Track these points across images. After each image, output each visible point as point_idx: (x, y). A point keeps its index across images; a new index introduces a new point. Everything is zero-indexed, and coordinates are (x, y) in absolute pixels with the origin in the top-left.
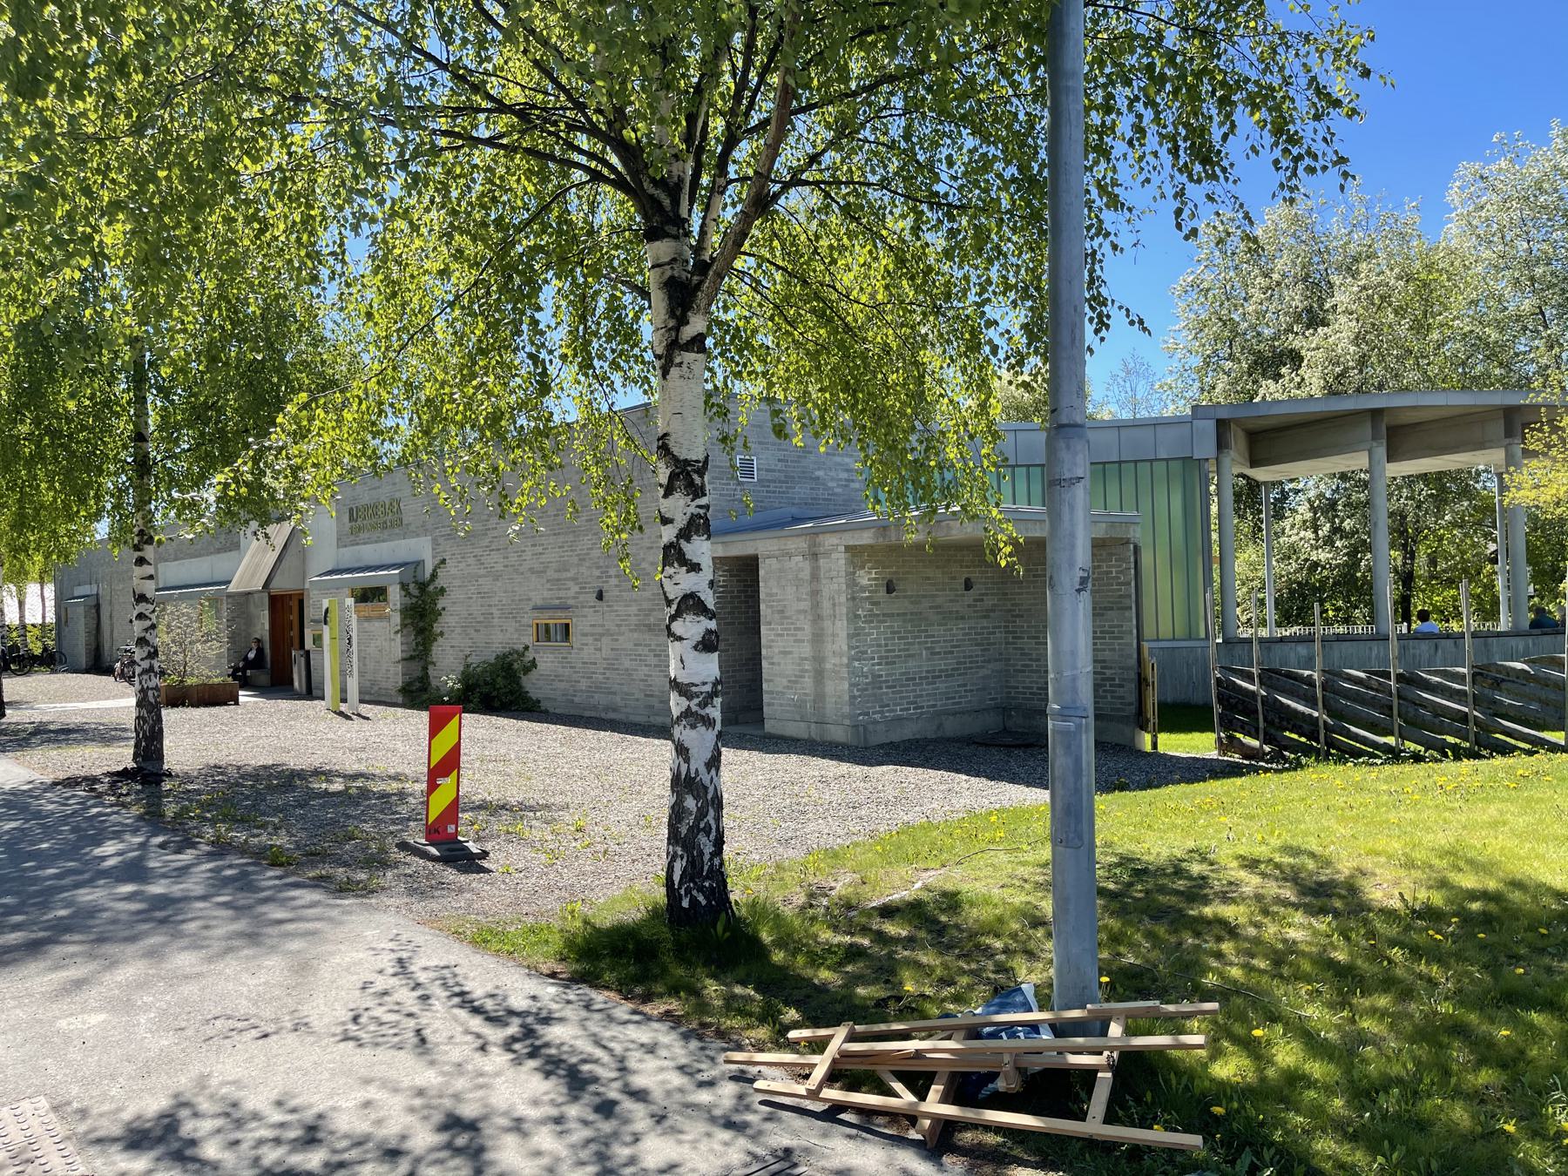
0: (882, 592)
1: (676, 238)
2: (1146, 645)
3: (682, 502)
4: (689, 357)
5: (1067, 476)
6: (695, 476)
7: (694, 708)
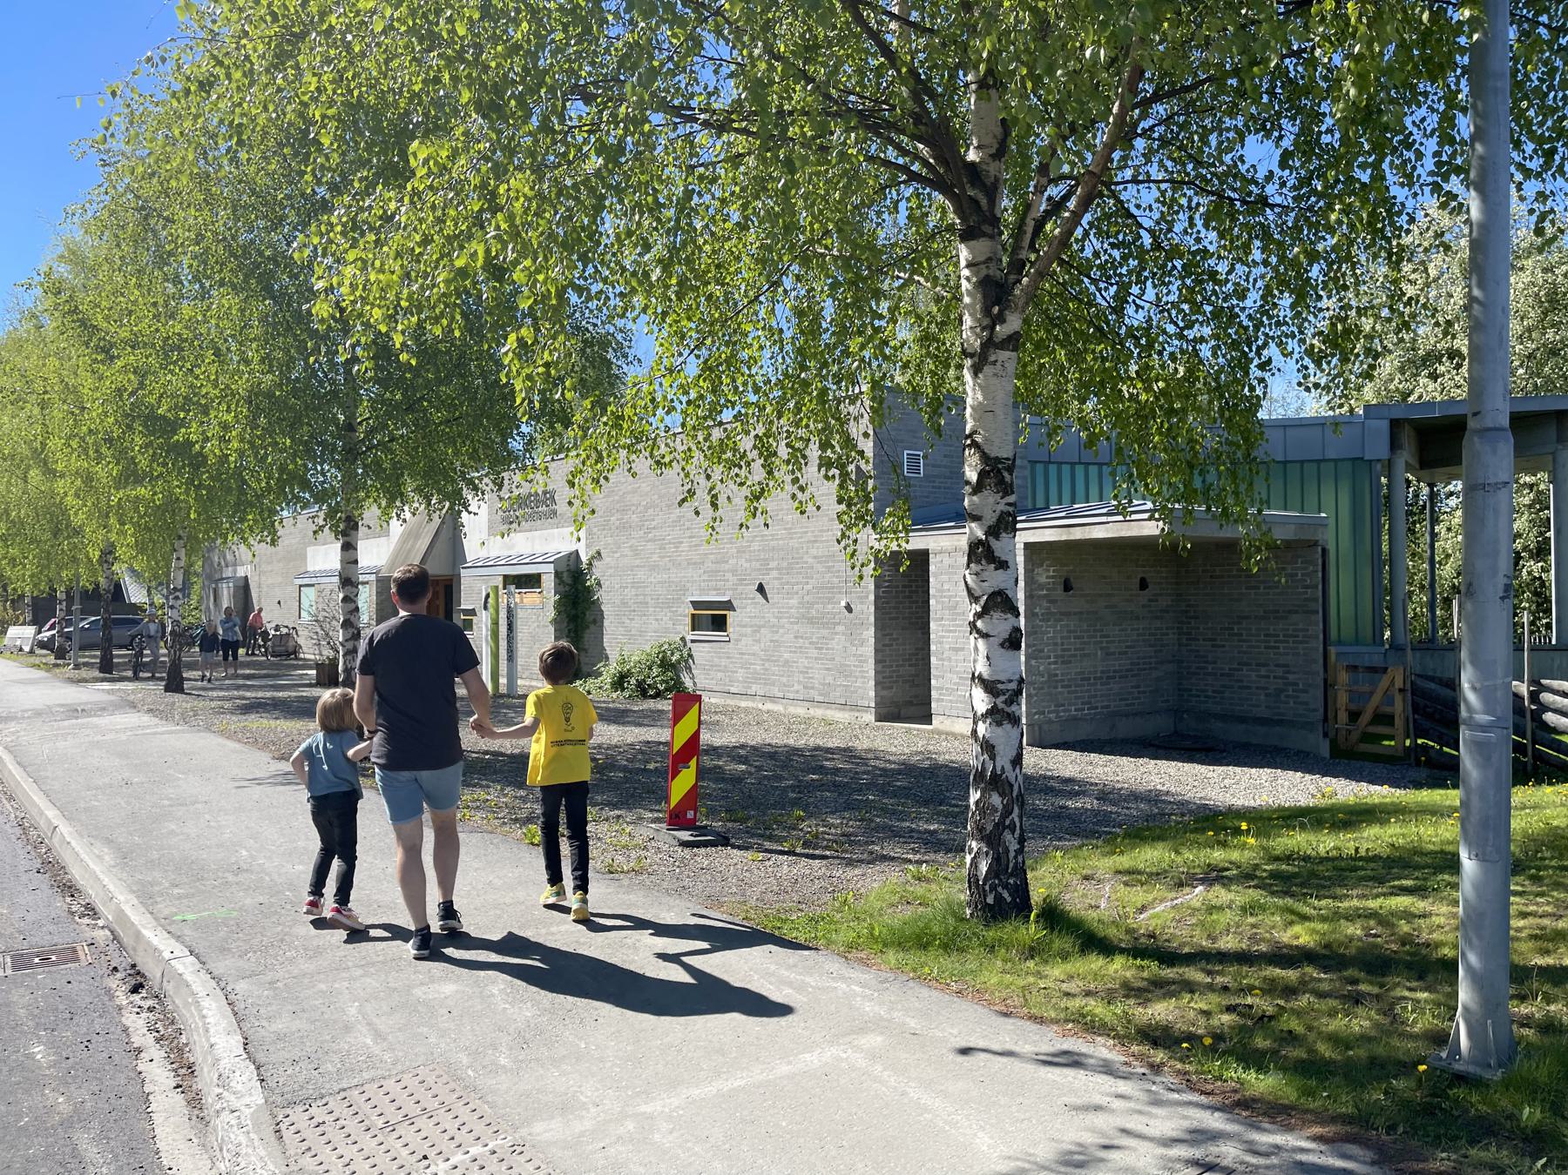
0: (1060, 591)
1: (992, 237)
2: (1332, 650)
3: (991, 500)
4: (1003, 355)
5: (1492, 481)
6: (1006, 474)
7: (1001, 706)
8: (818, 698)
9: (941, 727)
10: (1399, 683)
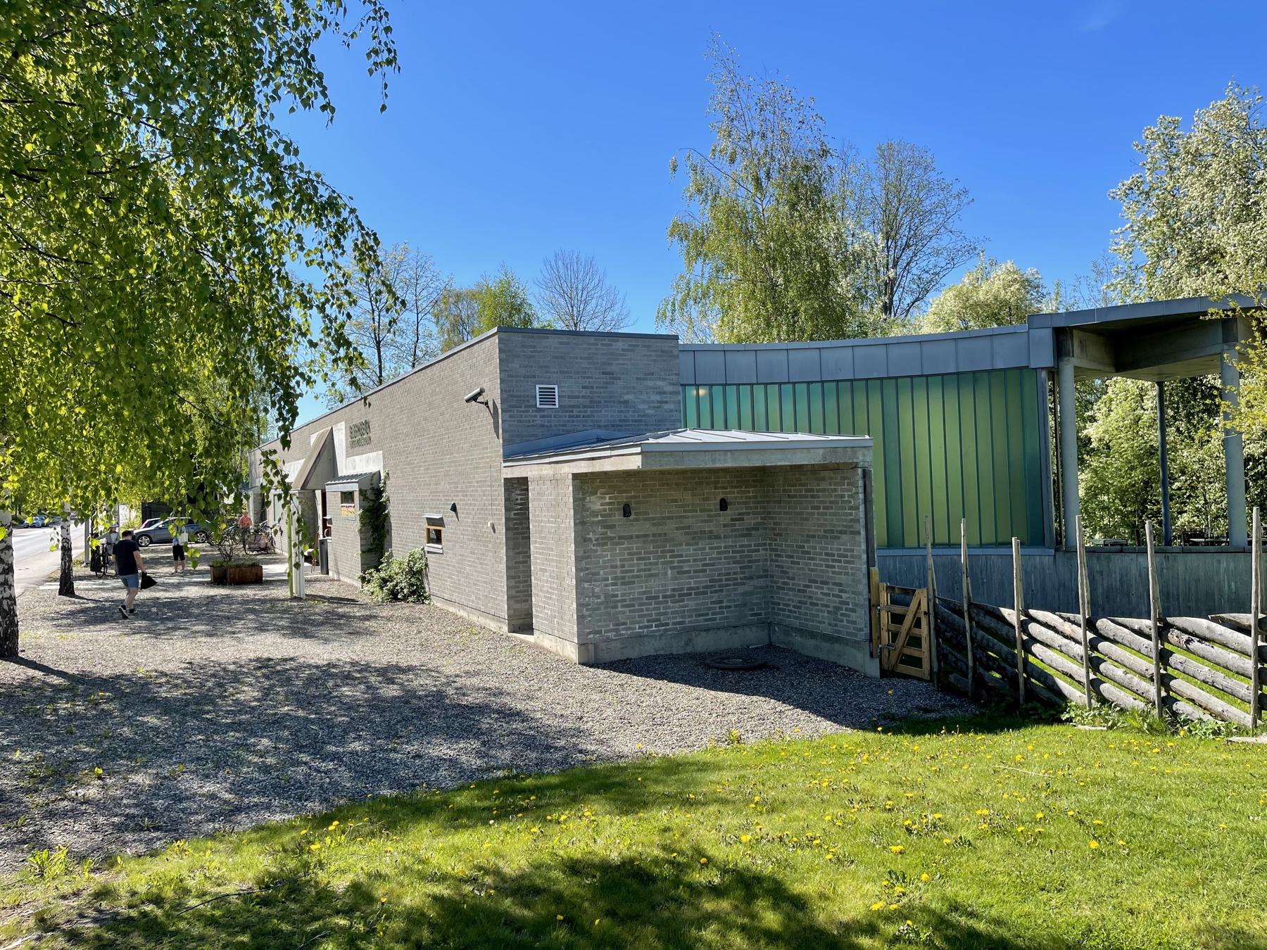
0: (618, 516)
8: (483, 608)
9: (540, 642)
10: (924, 607)
